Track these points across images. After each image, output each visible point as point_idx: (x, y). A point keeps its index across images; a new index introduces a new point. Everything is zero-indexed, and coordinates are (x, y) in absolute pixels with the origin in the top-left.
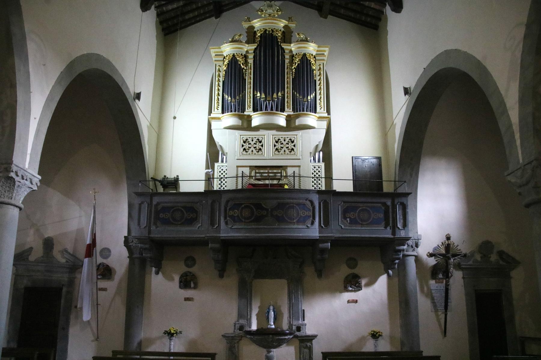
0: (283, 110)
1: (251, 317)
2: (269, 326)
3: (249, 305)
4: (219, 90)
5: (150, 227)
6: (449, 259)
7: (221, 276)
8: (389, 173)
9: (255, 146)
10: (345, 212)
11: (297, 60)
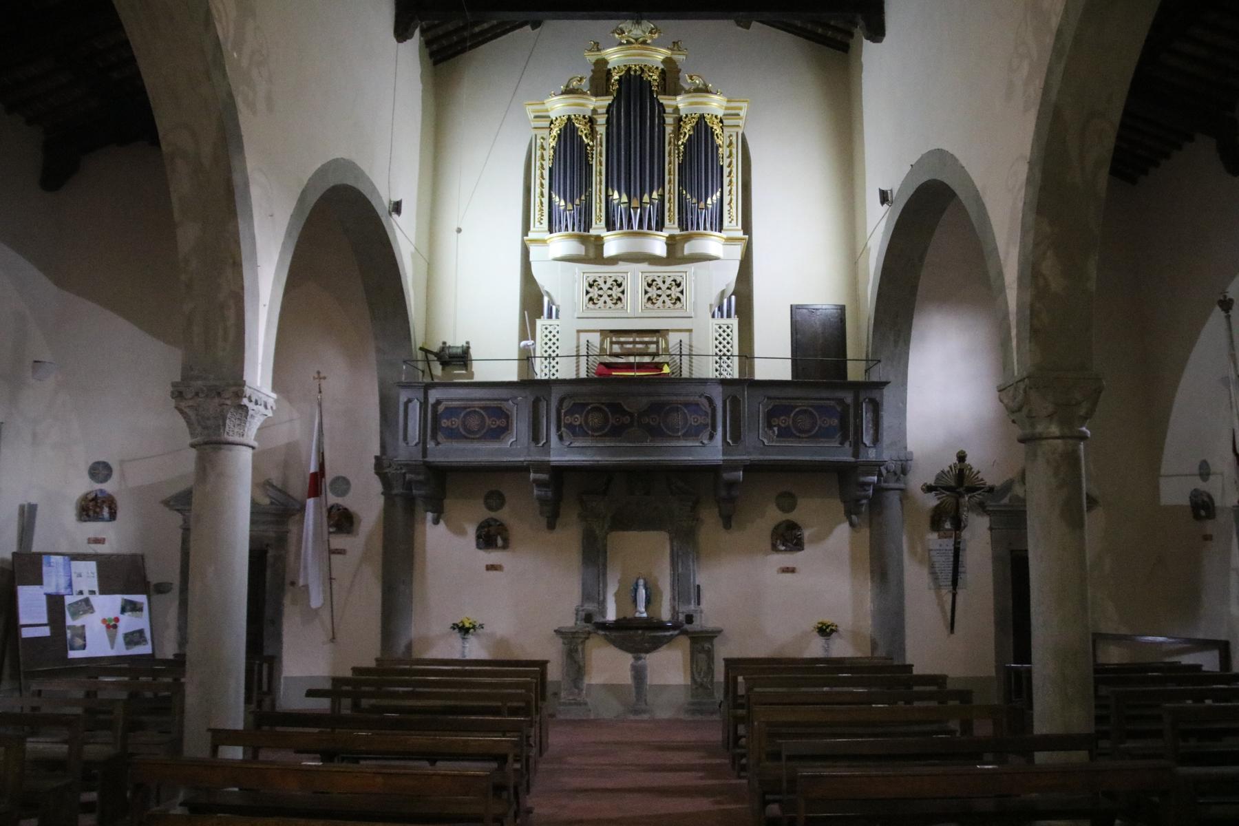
0: (660, 226)
1: (605, 599)
2: (637, 615)
3: (601, 577)
4: (542, 185)
5: (425, 443)
6: (961, 495)
7: (551, 526)
8: (857, 343)
9: (610, 292)
10: (771, 415)
11: (688, 127)
